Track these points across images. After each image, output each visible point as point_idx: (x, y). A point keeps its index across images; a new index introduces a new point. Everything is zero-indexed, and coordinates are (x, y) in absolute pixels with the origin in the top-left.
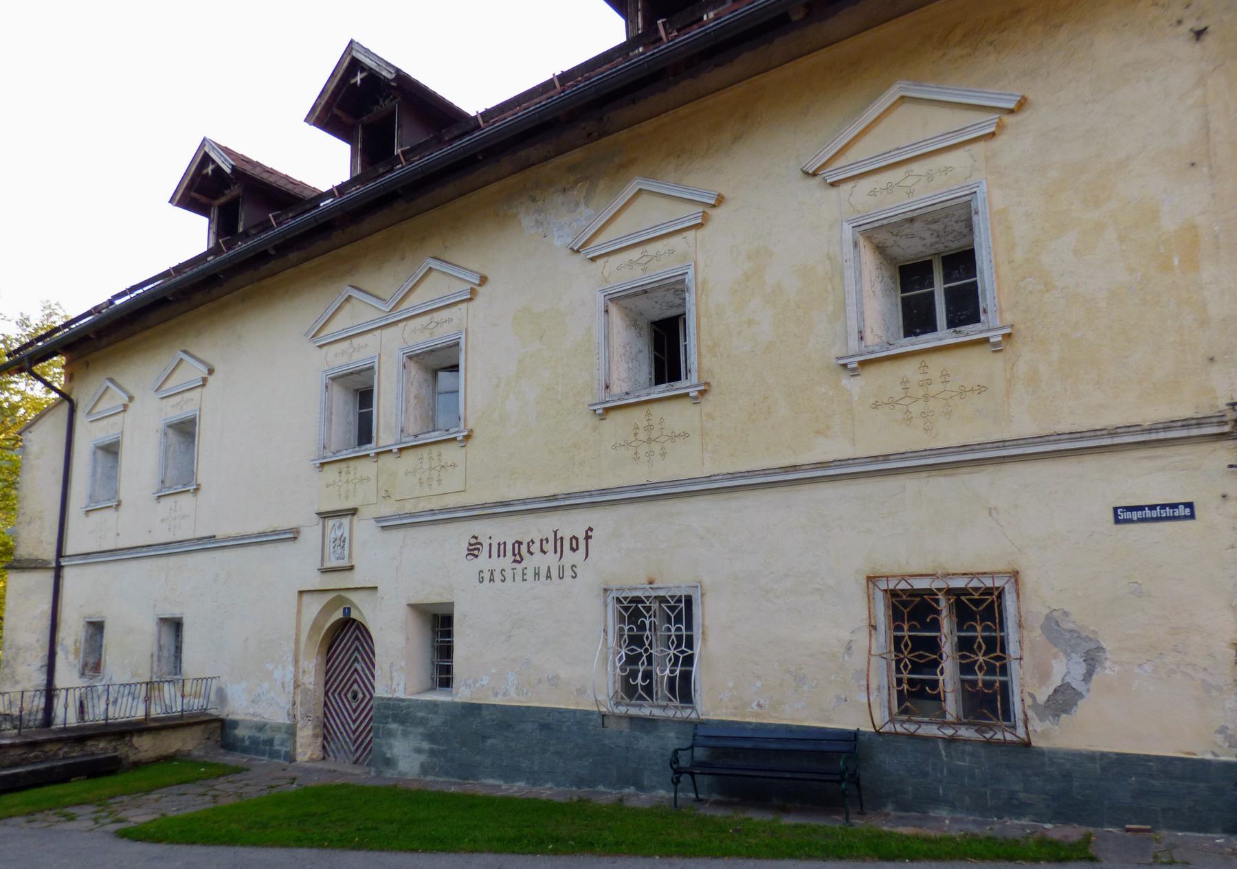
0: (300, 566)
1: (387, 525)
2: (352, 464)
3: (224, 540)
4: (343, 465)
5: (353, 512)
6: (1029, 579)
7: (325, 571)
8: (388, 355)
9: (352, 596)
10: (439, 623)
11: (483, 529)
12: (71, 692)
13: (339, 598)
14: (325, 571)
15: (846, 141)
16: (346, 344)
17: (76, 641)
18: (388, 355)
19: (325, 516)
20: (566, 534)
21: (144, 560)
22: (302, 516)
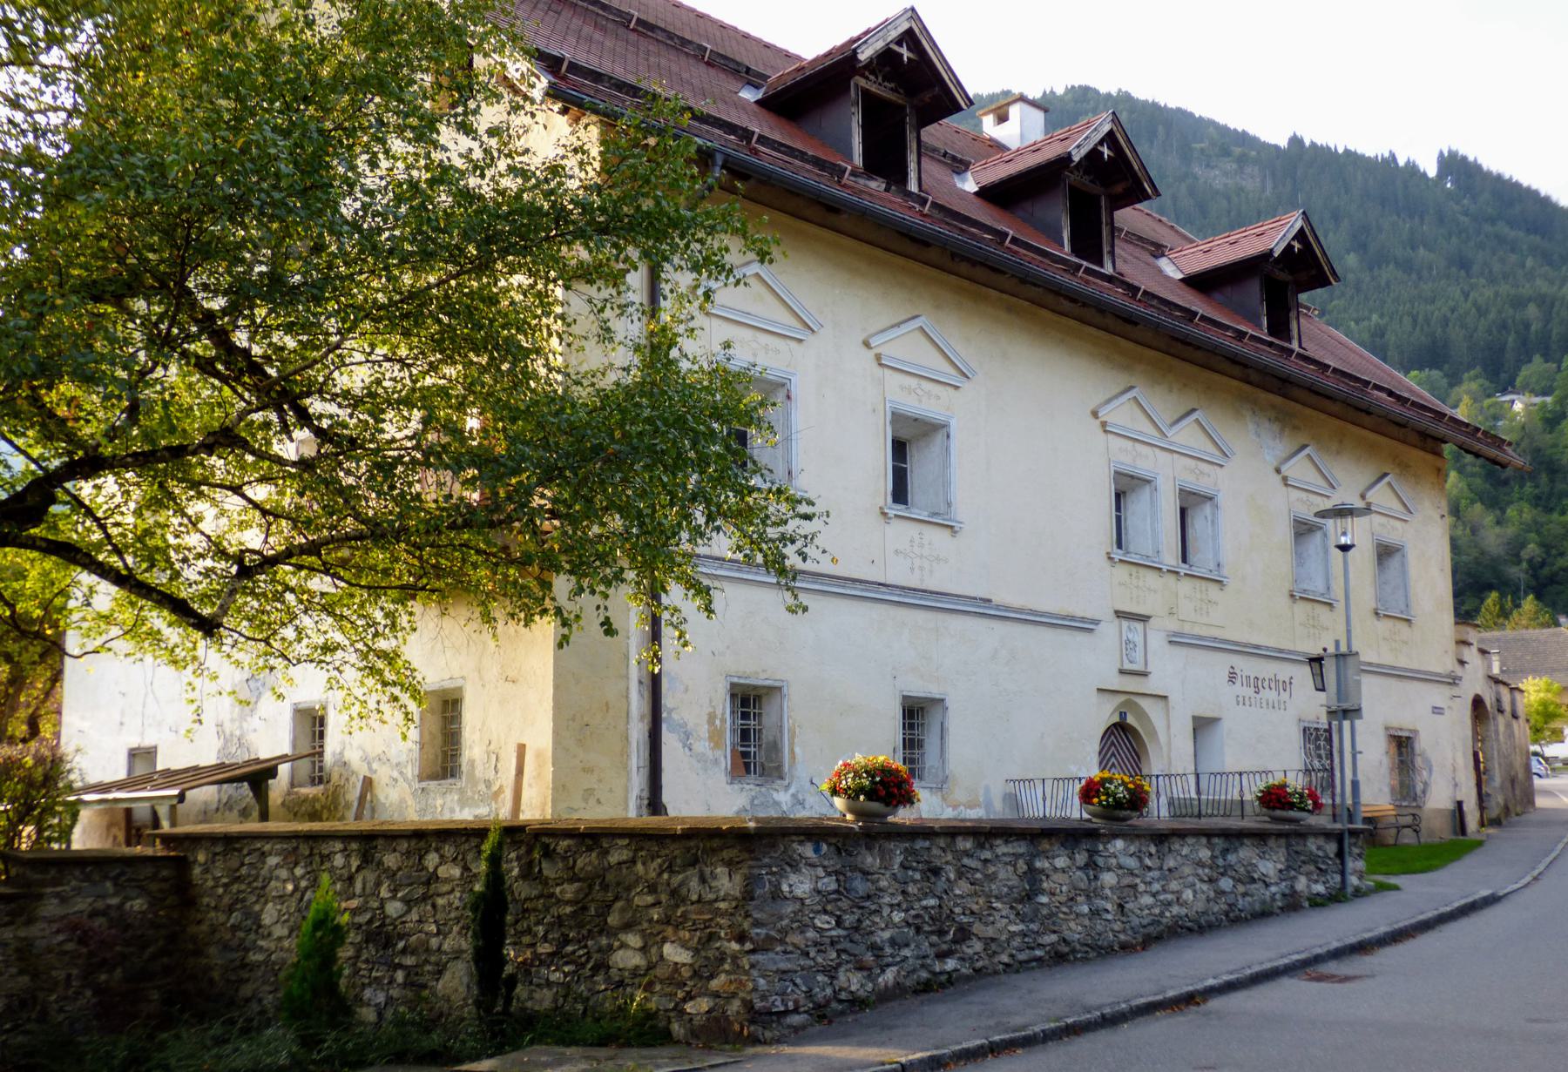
0: (1095, 661)
1: (1176, 640)
2: (1142, 571)
3: (998, 607)
4: (1134, 569)
5: (1143, 619)
6: (1225, 725)
7: (1122, 672)
8: (1168, 475)
9: (1145, 704)
10: (1202, 726)
11: (1240, 663)
12: (1245, 777)
13: (1129, 701)
14: (1122, 672)
15: (605, 66)
16: (1129, 444)
17: (711, 718)
18: (1168, 475)
19: (1119, 614)
20: (1281, 678)
21: (869, 604)
22: (1095, 604)
